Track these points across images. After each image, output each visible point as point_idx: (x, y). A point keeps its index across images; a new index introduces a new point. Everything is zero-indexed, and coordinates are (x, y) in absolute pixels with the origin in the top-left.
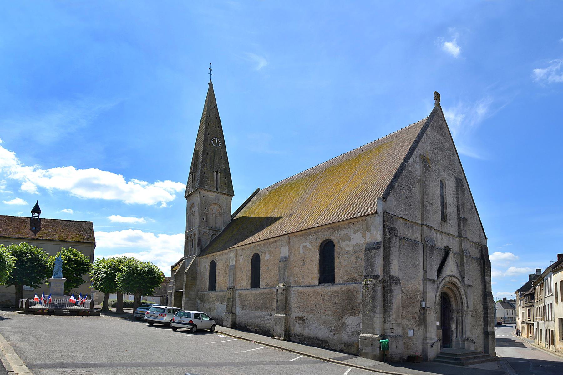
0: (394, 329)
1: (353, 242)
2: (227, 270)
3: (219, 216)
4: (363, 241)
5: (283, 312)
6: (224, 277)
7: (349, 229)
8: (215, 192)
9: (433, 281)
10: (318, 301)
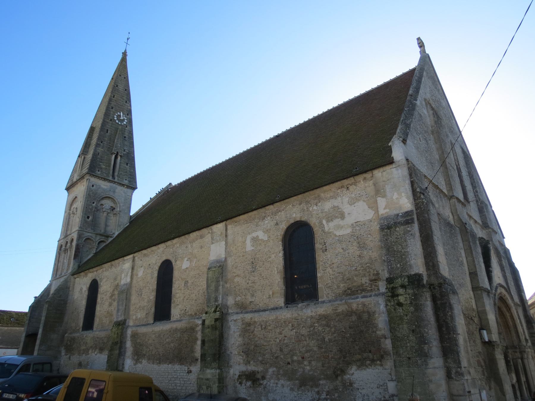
1: (349, 220)
2: (116, 293)
3: (112, 215)
4: (370, 215)
5: (215, 365)
6: (110, 305)
7: (339, 199)
8: (110, 181)
10: (286, 338)
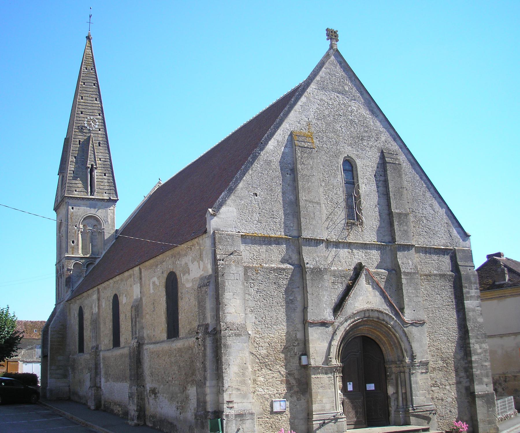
0: (235, 401)
3: (97, 234)
9: (324, 324)
